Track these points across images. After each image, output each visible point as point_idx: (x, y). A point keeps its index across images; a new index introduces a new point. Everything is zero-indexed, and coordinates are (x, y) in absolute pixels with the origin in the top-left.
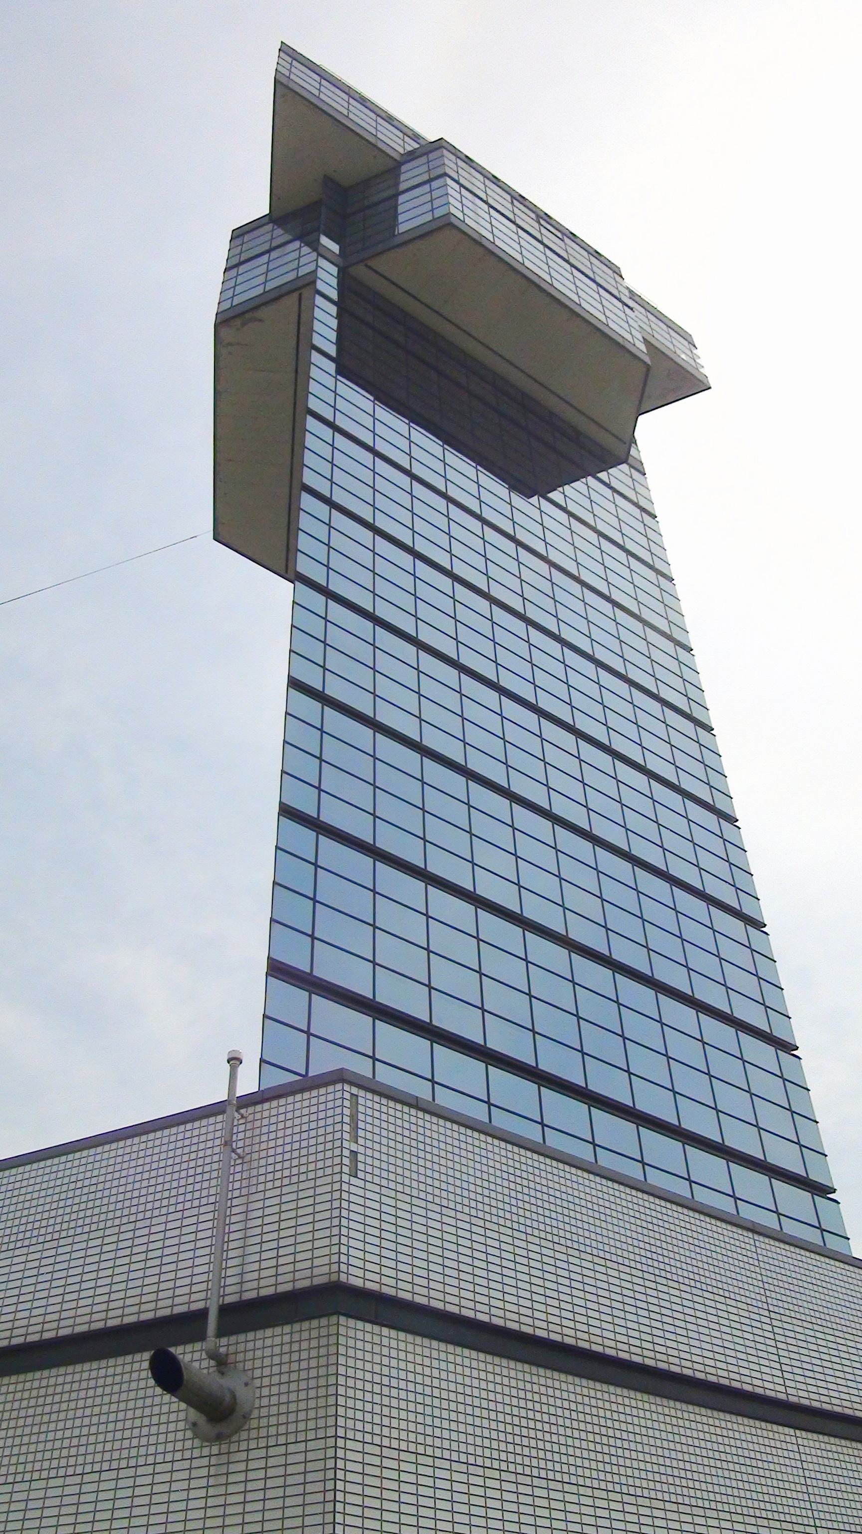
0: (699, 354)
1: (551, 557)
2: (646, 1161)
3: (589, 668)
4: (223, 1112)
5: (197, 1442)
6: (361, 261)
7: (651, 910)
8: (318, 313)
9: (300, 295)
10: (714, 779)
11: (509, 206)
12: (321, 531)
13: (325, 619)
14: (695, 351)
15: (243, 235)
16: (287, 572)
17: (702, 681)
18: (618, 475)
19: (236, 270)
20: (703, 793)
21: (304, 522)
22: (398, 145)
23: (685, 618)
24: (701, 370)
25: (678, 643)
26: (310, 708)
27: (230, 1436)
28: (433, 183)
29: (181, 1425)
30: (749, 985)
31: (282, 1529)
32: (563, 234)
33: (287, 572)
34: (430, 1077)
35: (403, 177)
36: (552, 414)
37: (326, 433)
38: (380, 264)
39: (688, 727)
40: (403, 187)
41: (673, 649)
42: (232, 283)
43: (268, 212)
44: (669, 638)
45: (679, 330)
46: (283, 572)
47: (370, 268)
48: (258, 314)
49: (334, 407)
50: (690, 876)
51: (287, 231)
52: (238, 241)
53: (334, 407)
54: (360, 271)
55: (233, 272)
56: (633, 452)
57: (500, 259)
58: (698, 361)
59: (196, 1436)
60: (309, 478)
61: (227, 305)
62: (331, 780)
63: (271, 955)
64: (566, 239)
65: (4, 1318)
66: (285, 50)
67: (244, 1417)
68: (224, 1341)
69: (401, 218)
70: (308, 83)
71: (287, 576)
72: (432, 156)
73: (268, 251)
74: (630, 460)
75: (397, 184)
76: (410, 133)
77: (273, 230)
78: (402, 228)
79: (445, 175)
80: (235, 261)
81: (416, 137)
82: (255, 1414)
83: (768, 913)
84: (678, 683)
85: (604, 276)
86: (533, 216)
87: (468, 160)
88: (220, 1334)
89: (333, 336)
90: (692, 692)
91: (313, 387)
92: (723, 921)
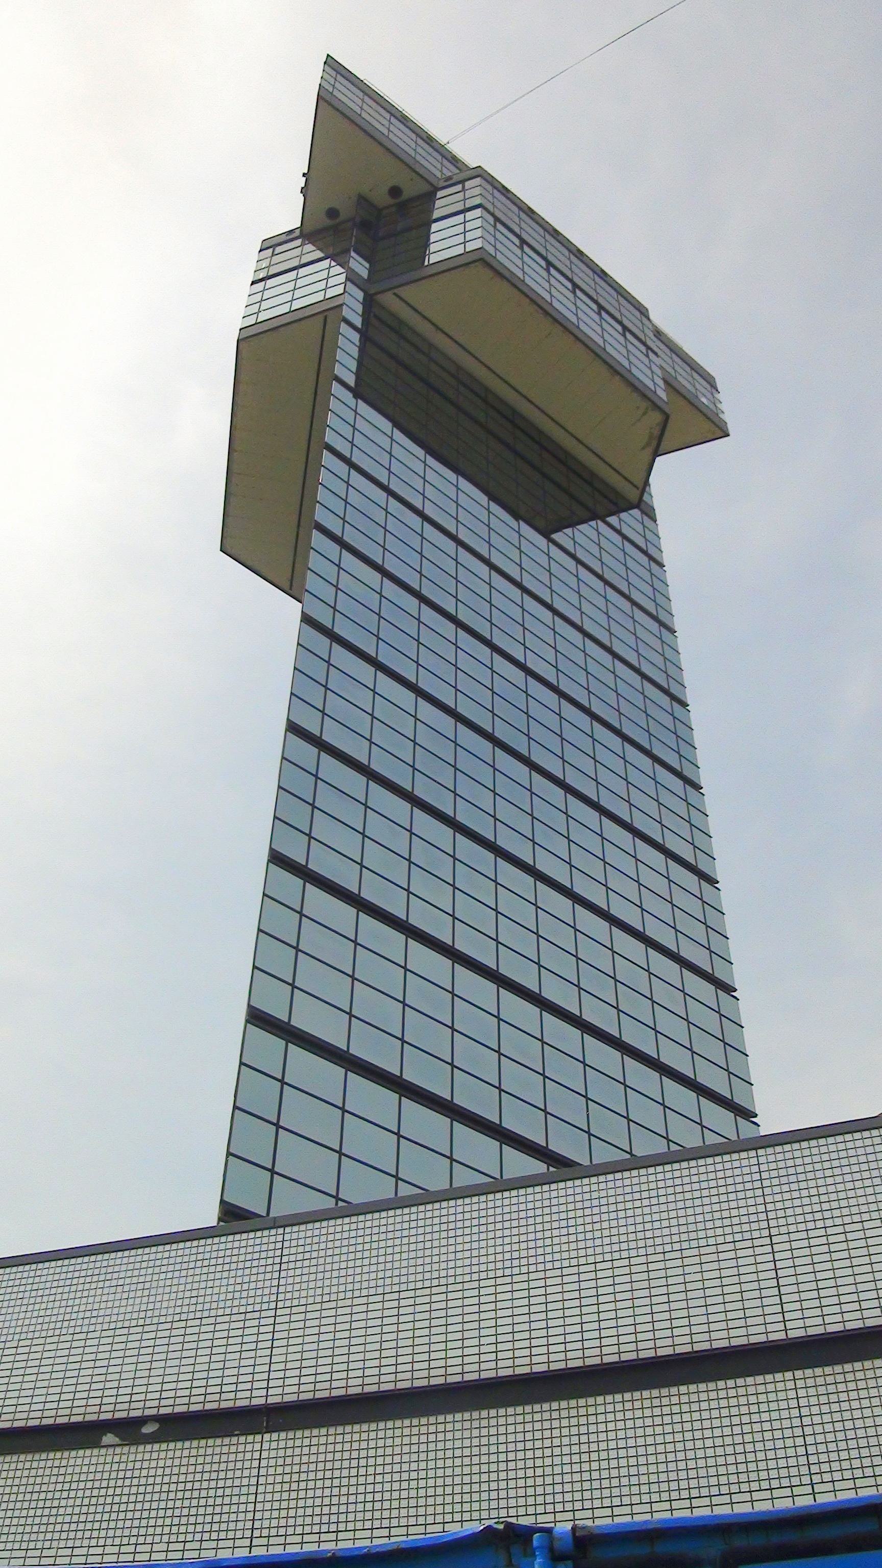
0: (723, 409)
1: (555, 606)
2: (458, 766)
3: (584, 721)
8: (341, 341)
10: (699, 839)
12: (330, 572)
13: (328, 662)
14: (716, 395)
15: (273, 247)
16: (291, 589)
17: (714, 846)
18: (629, 520)
20: (686, 853)
21: (314, 561)
22: (435, 168)
23: (672, 603)
24: (721, 416)
25: (673, 698)
26: (307, 753)
28: (462, 208)
30: (715, 1051)
33: (291, 589)
34: (298, 909)
35: (438, 203)
36: (566, 453)
37: (341, 468)
40: (436, 214)
42: (258, 297)
43: (299, 225)
44: (666, 692)
46: (287, 589)
49: (352, 443)
50: (666, 938)
53: (352, 443)
54: (388, 300)
56: (646, 497)
58: (719, 405)
60: (321, 516)
61: (251, 320)
62: (323, 828)
63: (251, 1003)
65: (3, 1366)
66: (330, 61)
69: (433, 248)
71: (290, 592)
74: (643, 506)
80: (262, 275)
81: (454, 160)
84: (659, 661)
85: (631, 319)
89: (353, 366)
90: (672, 670)
91: (331, 419)
92: (695, 984)
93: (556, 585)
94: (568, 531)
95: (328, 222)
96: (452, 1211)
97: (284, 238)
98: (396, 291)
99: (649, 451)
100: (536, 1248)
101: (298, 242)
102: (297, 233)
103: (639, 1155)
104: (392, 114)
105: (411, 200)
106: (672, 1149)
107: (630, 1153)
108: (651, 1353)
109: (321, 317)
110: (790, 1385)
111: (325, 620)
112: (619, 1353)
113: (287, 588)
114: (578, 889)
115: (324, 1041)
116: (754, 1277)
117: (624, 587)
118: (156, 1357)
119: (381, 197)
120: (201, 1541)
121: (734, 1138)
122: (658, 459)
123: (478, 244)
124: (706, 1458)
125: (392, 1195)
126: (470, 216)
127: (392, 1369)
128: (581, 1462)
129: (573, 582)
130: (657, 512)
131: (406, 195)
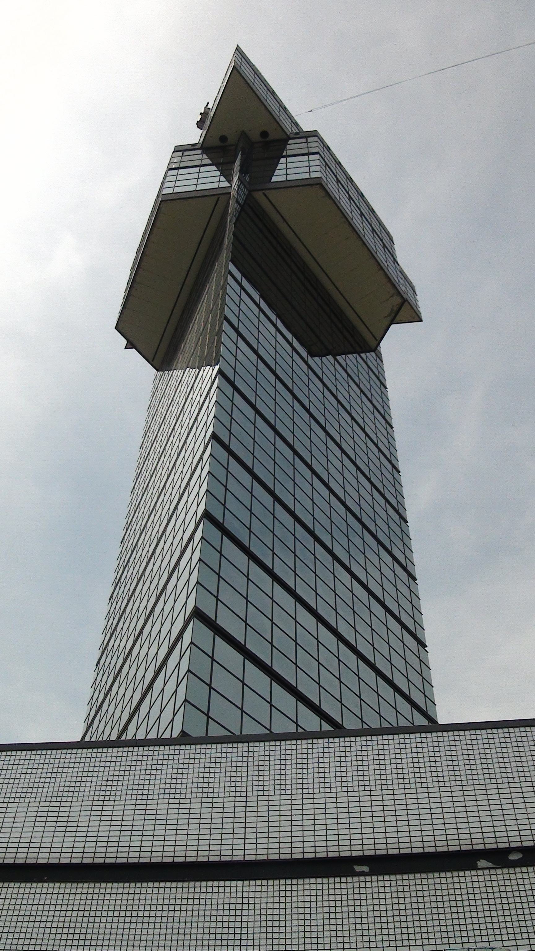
7: (255, 595)
9: (218, 198)
16: (153, 361)
18: (371, 356)
19: (198, 168)
22: (290, 129)
28: (202, 168)
33: (153, 361)
38: (269, 193)
41: (357, 460)
46: (151, 361)
54: (259, 196)
56: (378, 348)
74: (377, 351)
78: (274, 179)
81: (297, 125)
94: (344, 356)
95: (220, 144)
97: (190, 147)
98: (266, 192)
99: (389, 319)
100: (214, 782)
101: (200, 152)
102: (199, 146)
103: (275, 732)
104: (268, 89)
105: (274, 141)
106: (299, 731)
107: (270, 730)
109: (216, 197)
110: (240, 889)
111: (231, 376)
113: (151, 361)
115: (220, 626)
116: (312, 812)
119: (255, 136)
121: (238, 733)
122: (392, 326)
123: (317, 175)
125: (169, 737)
126: (312, 157)
127: (104, 850)
128: (273, 903)
130: (383, 356)
131: (271, 137)
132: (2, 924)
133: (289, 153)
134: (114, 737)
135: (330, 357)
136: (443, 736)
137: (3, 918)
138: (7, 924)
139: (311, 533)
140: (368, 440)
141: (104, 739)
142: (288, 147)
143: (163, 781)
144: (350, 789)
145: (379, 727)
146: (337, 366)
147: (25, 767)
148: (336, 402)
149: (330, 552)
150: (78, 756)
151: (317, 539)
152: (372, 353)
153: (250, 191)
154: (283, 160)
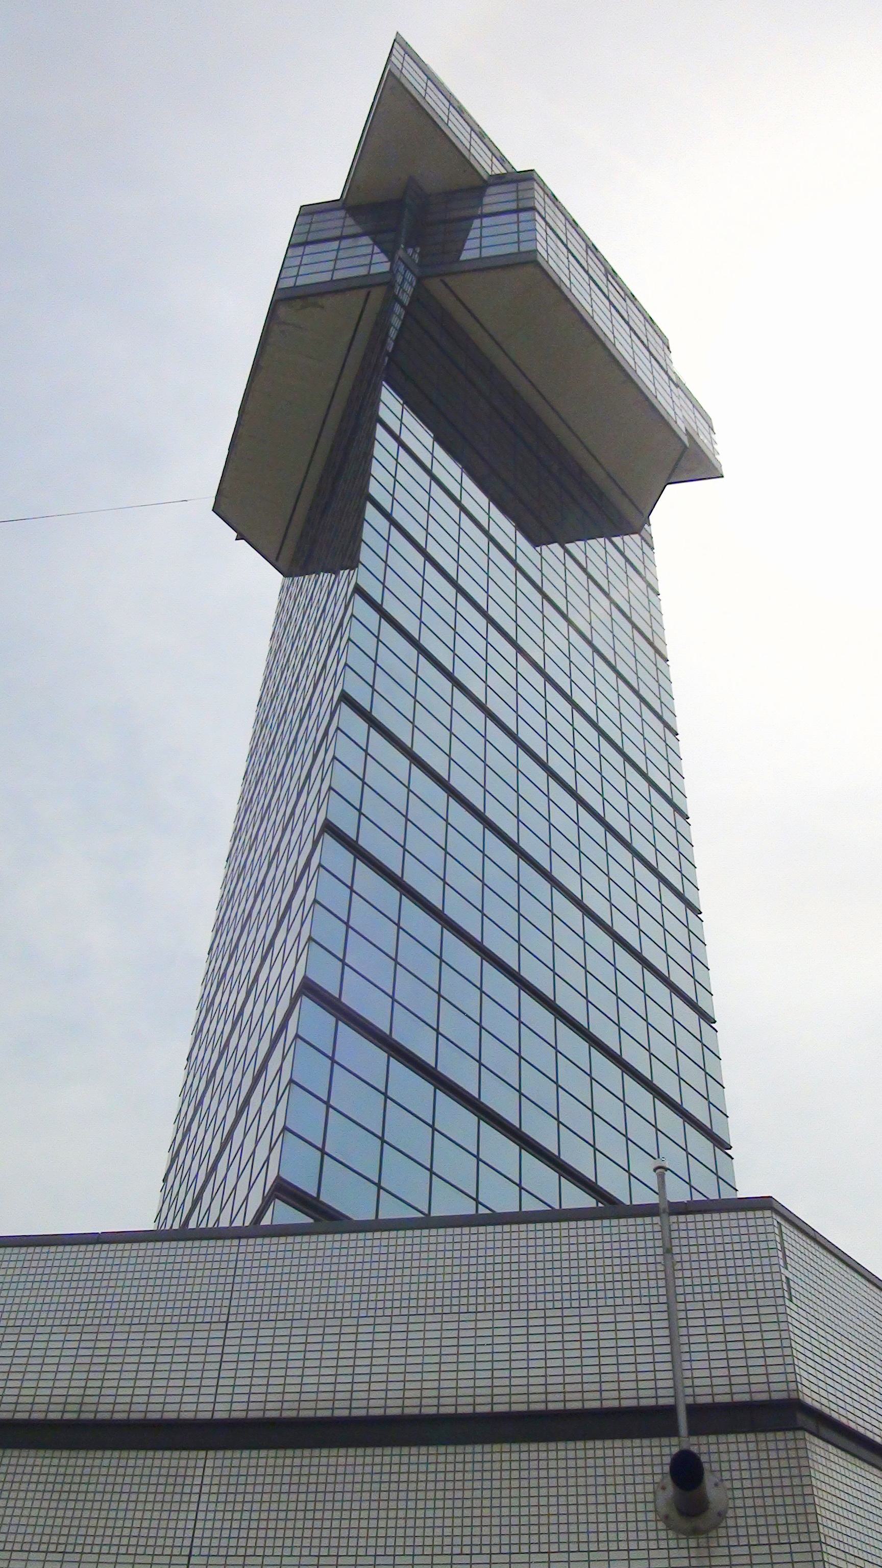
4: (656, 1214)
5: (671, 1534)
6: (439, 275)
11: (584, 254)
14: (713, 436)
16: (277, 559)
18: (631, 542)
22: (488, 166)
24: (717, 457)
27: (706, 1532)
29: (651, 1516)
31: (356, 1565)
32: (626, 294)
33: (277, 559)
38: (452, 281)
39: (668, 810)
45: (704, 414)
47: (446, 285)
48: (323, 301)
51: (358, 223)
52: (307, 219)
54: (435, 285)
55: (299, 251)
57: (575, 309)
58: (715, 446)
59: (669, 1528)
64: (627, 299)
66: (399, 41)
67: (719, 1514)
68: (694, 1439)
70: (414, 80)
71: (276, 563)
72: (522, 186)
73: (340, 238)
74: (643, 533)
75: (481, 205)
76: (498, 155)
77: (345, 218)
79: (533, 209)
81: (503, 160)
82: (730, 1513)
83: (718, 1008)
86: (603, 269)
87: (554, 199)
88: (692, 1432)
93: (428, 616)
96: (289, 1247)
108: (560, 1406)
112: (510, 1403)
114: (436, 926)
117: (510, 629)
118: (34, 1353)
120: (100, 1554)
121: (557, 1207)
122: (668, 486)
124: (588, 1523)
129: (449, 614)
132: (2, 1538)
133: (487, 210)
134: (176, 1226)
135: (555, 547)
136: (704, 1221)
137: (5, 1529)
138: (11, 1538)
139: (547, 875)
140: (645, 709)
141: (210, 1225)
142: (486, 200)
143: (406, 1279)
144: (636, 1301)
145: (717, 1198)
146: (570, 563)
147: (93, 1269)
148: (614, 676)
149: (578, 903)
150: (274, 1248)
151: (555, 884)
152: (633, 536)
153: (419, 280)
154: (476, 223)
